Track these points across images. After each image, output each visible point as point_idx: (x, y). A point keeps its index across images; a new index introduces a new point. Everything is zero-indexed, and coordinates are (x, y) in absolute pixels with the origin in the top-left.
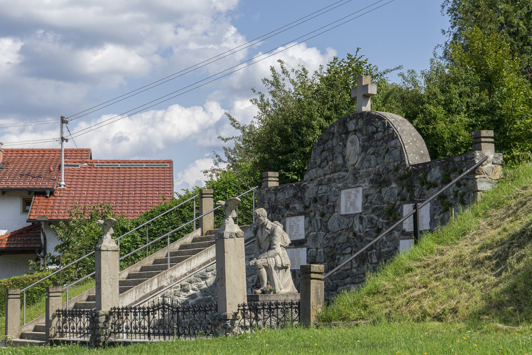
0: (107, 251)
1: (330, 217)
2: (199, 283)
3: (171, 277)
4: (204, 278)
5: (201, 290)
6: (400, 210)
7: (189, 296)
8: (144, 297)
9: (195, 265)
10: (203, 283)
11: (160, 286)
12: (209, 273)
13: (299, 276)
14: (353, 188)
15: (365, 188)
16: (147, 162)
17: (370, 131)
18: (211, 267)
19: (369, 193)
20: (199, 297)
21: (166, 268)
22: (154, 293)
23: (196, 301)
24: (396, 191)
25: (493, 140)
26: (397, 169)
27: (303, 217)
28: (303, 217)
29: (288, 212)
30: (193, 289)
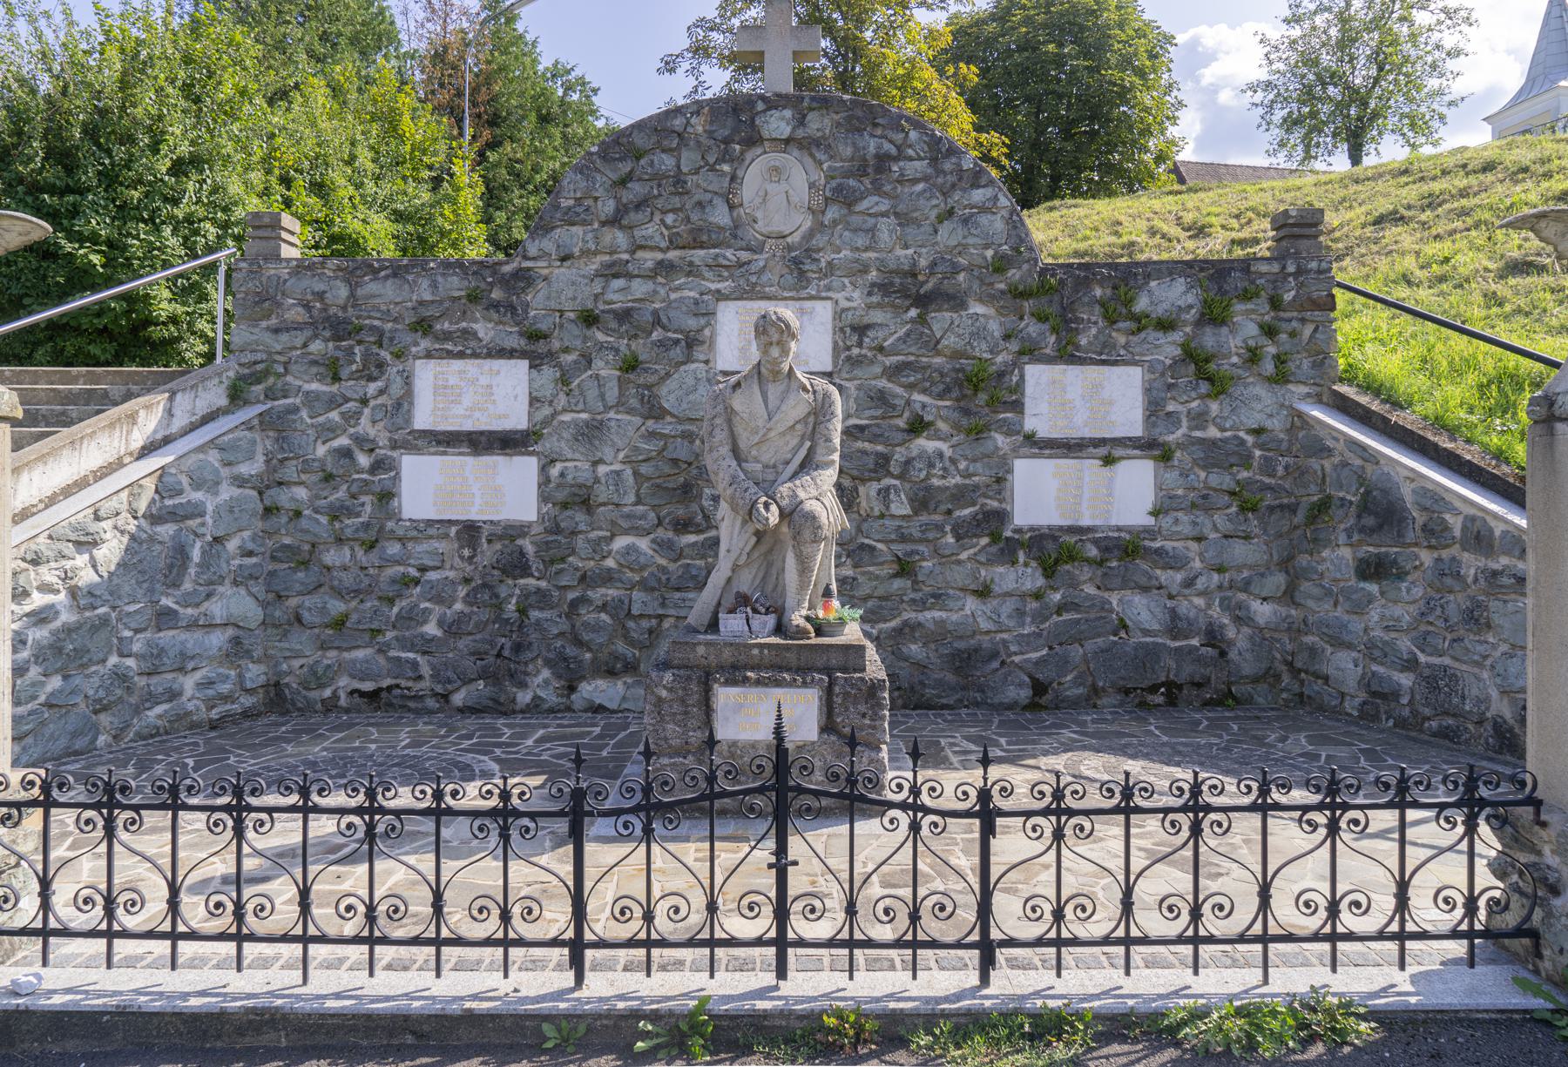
1: (668, 375)
2: (68, 564)
4: (87, 543)
5: (73, 592)
7: (27, 615)
9: (35, 492)
10: (82, 560)
12: (104, 524)
13: (489, 541)
14: (786, 299)
15: (844, 304)
17: (872, 150)
18: (113, 504)
19: (866, 320)
20: (66, 617)
23: (53, 633)
24: (995, 328)
25: (284, 235)
26: (1001, 265)
27: (526, 363)
28: (526, 363)
29: (425, 344)
30: (45, 588)
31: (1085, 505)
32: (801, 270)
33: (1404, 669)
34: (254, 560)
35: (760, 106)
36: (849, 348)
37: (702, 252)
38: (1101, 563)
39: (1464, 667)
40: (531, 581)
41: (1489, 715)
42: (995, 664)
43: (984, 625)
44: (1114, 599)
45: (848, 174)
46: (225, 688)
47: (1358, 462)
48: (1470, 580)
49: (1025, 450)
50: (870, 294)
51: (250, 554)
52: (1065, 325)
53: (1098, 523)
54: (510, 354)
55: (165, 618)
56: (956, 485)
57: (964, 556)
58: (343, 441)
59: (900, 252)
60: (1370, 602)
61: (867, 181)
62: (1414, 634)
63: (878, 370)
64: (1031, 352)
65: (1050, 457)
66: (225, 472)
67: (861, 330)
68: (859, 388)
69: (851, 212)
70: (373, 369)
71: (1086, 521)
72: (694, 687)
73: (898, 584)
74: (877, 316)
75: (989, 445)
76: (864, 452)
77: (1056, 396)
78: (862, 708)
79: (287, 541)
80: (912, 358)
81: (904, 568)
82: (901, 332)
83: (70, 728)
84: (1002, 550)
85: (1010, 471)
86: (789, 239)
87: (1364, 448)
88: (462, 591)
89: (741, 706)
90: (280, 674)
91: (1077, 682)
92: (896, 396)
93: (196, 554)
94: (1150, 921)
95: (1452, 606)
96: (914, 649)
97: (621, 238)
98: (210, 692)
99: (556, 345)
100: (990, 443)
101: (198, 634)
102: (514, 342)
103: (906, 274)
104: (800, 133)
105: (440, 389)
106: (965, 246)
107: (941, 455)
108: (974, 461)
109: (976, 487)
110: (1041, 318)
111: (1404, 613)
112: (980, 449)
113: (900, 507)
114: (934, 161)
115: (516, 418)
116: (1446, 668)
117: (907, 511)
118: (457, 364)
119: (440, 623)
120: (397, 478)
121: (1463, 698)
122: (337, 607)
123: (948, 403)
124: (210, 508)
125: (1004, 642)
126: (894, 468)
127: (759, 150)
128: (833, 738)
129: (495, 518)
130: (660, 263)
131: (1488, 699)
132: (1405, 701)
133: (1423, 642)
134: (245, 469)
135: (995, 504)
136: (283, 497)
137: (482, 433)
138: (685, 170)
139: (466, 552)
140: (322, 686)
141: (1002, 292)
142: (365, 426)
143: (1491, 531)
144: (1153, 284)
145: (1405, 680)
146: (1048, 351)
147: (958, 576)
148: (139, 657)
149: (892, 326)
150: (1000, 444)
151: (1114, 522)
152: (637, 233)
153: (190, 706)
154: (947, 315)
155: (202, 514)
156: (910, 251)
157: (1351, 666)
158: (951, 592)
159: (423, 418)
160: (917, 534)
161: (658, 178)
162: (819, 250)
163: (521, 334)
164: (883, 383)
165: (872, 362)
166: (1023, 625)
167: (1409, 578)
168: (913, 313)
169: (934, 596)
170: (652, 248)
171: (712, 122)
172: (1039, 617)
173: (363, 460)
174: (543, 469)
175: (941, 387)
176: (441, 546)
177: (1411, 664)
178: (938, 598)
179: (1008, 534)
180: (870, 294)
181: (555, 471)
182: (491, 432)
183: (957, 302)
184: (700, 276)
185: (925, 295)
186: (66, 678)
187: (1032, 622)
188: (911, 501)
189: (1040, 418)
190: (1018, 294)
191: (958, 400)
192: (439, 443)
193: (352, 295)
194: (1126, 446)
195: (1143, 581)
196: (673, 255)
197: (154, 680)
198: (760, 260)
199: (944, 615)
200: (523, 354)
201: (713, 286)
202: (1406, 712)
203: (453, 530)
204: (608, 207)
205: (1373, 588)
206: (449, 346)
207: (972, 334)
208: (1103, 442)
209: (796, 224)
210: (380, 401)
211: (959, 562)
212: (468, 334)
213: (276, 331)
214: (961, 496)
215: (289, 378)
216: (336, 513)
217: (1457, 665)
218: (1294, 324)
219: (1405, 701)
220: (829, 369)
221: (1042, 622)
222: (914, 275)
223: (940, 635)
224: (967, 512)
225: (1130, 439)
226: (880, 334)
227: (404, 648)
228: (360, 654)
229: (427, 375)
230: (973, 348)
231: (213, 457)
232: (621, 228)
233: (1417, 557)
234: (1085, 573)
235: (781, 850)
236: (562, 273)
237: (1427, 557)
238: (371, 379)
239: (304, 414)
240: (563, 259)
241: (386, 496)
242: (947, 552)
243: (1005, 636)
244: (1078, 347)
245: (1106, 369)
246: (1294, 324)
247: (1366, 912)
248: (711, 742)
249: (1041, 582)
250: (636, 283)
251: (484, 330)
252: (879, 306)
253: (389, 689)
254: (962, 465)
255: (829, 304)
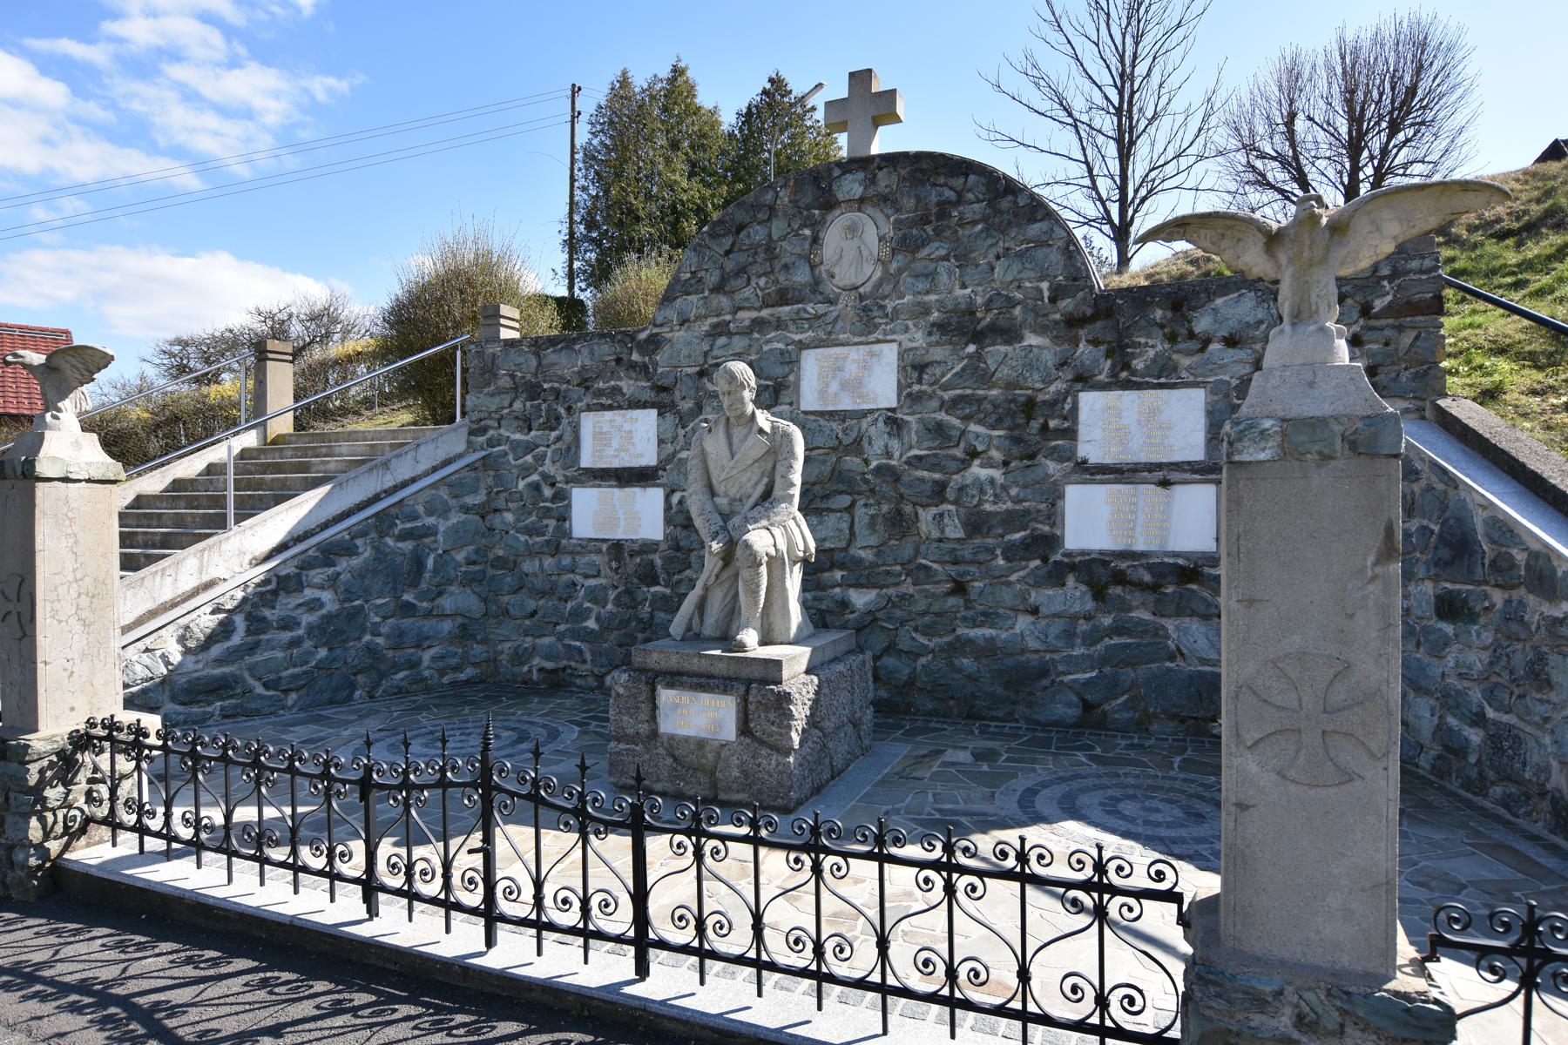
0: (66, 480)
3: (242, 553)
6: (1067, 407)
8: (152, 614)
11: (206, 578)
16: (20, 327)
17: (934, 199)
19: (927, 359)
21: (220, 523)
22: (184, 601)
24: (1049, 359)
25: (502, 321)
27: (654, 412)
28: (654, 412)
29: (587, 400)
31: (1139, 530)
32: (869, 318)
33: (1473, 724)
34: (477, 568)
35: (837, 172)
36: (910, 386)
37: (787, 308)
38: (1154, 588)
39: (1528, 729)
40: (658, 588)
41: (1548, 786)
42: (1045, 682)
43: (1032, 644)
44: (1170, 625)
45: (912, 224)
46: (454, 661)
47: (1440, 487)
48: (1533, 628)
49: (1074, 477)
50: (930, 334)
51: (474, 563)
52: (1120, 353)
53: (1153, 548)
54: (644, 405)
55: (408, 609)
56: (1007, 511)
57: (1013, 578)
58: (535, 477)
59: (959, 292)
60: (1446, 645)
61: (929, 229)
62: (1485, 685)
63: (935, 404)
64: (1084, 380)
65: (1102, 482)
66: (452, 502)
67: (921, 368)
68: (921, 421)
69: (914, 260)
70: (553, 422)
71: (1140, 546)
72: (643, 687)
73: (952, 601)
74: (938, 354)
75: (1039, 471)
76: (922, 480)
77: (1109, 421)
78: (772, 716)
79: (501, 553)
80: (969, 391)
81: (960, 588)
82: (958, 368)
83: (333, 684)
84: (1050, 573)
85: (1062, 496)
86: (861, 290)
87: (1444, 471)
88: (612, 595)
89: (678, 706)
90: (496, 653)
91: (1125, 706)
92: (954, 427)
93: (430, 563)
94: (777, 949)
95: (1519, 656)
96: (966, 662)
97: (724, 301)
98: (441, 664)
99: (677, 394)
100: (1039, 470)
101: (433, 622)
102: (648, 395)
103: (964, 313)
104: (871, 192)
105: (598, 435)
106: (1021, 280)
107: (992, 481)
108: (1025, 487)
109: (1027, 512)
110: (1095, 342)
111: (1477, 660)
112: (1031, 476)
113: (954, 531)
114: (992, 203)
115: (647, 456)
116: (1510, 727)
117: (960, 534)
118: (608, 415)
119: (598, 619)
120: (569, 506)
121: (1524, 764)
122: (531, 604)
123: (1001, 433)
124: (441, 529)
125: (1054, 661)
126: (950, 494)
127: (838, 212)
128: (748, 740)
129: (634, 537)
130: (754, 321)
131: (1547, 769)
132: (1473, 759)
133: (1490, 695)
134: (469, 500)
135: (1047, 528)
136: (496, 520)
137: (625, 469)
138: (775, 237)
139: (614, 564)
140: (522, 664)
141: (1056, 323)
142: (548, 467)
143: (1554, 570)
144: (1219, 301)
145: (1475, 736)
146: (1101, 377)
147: (1007, 596)
148: (388, 637)
149: (950, 360)
150: (1051, 471)
151: (1170, 548)
152: (737, 296)
153: (426, 673)
154: (1003, 348)
155: (435, 534)
156: (969, 290)
157: (1428, 715)
158: (1001, 611)
159: (586, 461)
160: (968, 556)
161: (754, 249)
162: (885, 297)
163: (651, 388)
164: (942, 416)
165: (931, 397)
166: (1072, 646)
167: (1482, 620)
168: (971, 348)
169: (984, 614)
170: (749, 309)
171: (796, 193)
172: (1092, 638)
173: (548, 492)
174: (667, 497)
175: (994, 417)
176: (597, 558)
177: (1479, 720)
178: (988, 618)
179: (1058, 557)
180: (930, 334)
181: (675, 498)
182: (631, 469)
183: (1010, 334)
184: (786, 328)
185: (981, 332)
186: (330, 649)
187: (1083, 644)
188: (965, 525)
189: (1092, 448)
190: (1073, 322)
191: (1009, 429)
192: (595, 478)
193: (540, 364)
194: (1185, 471)
195: (1202, 609)
196: (765, 313)
197: (398, 653)
198: (834, 311)
199: (993, 632)
200: (651, 405)
201: (797, 337)
202: (1474, 774)
203: (604, 547)
204: (713, 278)
205: (1448, 628)
206: (603, 401)
207: (1024, 366)
208: (1159, 466)
209: (868, 274)
210: (558, 445)
211: (1009, 584)
212: (616, 390)
213: (493, 395)
214: (1012, 520)
215: (502, 431)
216: (530, 531)
217: (1521, 725)
218: (1388, 332)
219: (1473, 759)
220: (894, 405)
221: (1091, 645)
222: (973, 313)
223: (989, 650)
224: (1018, 536)
225: (1189, 463)
226: (938, 371)
227: (574, 639)
228: (546, 640)
229: (590, 423)
230: (1025, 379)
231: (444, 493)
232: (725, 293)
233: (1486, 596)
234: (1136, 598)
235: (488, 839)
236: (680, 335)
237: (1498, 597)
238: (553, 429)
239: (511, 457)
240: (682, 324)
241: (564, 517)
242: (997, 573)
243: (1056, 656)
244: (1134, 372)
245: (1165, 393)
246: (1388, 332)
247: (982, 984)
248: (654, 734)
249: (1090, 605)
250: (736, 339)
251: (628, 385)
252: (938, 344)
253: (564, 669)
254: (1014, 492)
255: (895, 346)
